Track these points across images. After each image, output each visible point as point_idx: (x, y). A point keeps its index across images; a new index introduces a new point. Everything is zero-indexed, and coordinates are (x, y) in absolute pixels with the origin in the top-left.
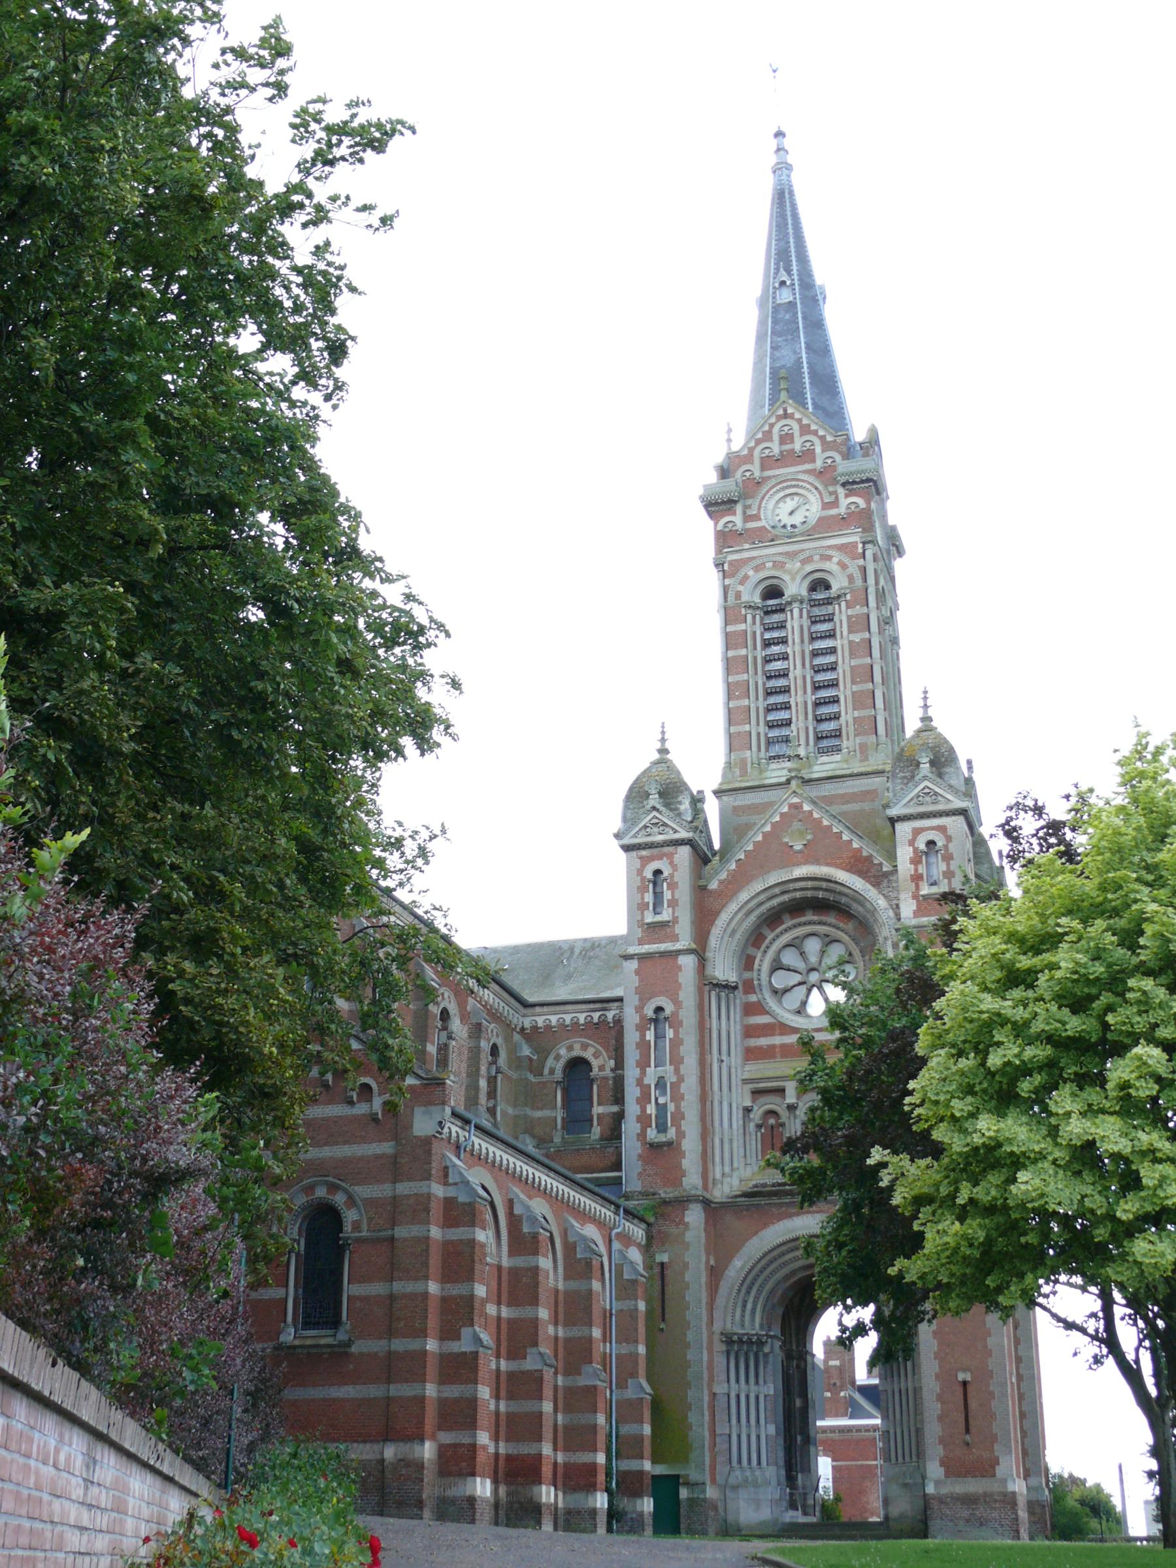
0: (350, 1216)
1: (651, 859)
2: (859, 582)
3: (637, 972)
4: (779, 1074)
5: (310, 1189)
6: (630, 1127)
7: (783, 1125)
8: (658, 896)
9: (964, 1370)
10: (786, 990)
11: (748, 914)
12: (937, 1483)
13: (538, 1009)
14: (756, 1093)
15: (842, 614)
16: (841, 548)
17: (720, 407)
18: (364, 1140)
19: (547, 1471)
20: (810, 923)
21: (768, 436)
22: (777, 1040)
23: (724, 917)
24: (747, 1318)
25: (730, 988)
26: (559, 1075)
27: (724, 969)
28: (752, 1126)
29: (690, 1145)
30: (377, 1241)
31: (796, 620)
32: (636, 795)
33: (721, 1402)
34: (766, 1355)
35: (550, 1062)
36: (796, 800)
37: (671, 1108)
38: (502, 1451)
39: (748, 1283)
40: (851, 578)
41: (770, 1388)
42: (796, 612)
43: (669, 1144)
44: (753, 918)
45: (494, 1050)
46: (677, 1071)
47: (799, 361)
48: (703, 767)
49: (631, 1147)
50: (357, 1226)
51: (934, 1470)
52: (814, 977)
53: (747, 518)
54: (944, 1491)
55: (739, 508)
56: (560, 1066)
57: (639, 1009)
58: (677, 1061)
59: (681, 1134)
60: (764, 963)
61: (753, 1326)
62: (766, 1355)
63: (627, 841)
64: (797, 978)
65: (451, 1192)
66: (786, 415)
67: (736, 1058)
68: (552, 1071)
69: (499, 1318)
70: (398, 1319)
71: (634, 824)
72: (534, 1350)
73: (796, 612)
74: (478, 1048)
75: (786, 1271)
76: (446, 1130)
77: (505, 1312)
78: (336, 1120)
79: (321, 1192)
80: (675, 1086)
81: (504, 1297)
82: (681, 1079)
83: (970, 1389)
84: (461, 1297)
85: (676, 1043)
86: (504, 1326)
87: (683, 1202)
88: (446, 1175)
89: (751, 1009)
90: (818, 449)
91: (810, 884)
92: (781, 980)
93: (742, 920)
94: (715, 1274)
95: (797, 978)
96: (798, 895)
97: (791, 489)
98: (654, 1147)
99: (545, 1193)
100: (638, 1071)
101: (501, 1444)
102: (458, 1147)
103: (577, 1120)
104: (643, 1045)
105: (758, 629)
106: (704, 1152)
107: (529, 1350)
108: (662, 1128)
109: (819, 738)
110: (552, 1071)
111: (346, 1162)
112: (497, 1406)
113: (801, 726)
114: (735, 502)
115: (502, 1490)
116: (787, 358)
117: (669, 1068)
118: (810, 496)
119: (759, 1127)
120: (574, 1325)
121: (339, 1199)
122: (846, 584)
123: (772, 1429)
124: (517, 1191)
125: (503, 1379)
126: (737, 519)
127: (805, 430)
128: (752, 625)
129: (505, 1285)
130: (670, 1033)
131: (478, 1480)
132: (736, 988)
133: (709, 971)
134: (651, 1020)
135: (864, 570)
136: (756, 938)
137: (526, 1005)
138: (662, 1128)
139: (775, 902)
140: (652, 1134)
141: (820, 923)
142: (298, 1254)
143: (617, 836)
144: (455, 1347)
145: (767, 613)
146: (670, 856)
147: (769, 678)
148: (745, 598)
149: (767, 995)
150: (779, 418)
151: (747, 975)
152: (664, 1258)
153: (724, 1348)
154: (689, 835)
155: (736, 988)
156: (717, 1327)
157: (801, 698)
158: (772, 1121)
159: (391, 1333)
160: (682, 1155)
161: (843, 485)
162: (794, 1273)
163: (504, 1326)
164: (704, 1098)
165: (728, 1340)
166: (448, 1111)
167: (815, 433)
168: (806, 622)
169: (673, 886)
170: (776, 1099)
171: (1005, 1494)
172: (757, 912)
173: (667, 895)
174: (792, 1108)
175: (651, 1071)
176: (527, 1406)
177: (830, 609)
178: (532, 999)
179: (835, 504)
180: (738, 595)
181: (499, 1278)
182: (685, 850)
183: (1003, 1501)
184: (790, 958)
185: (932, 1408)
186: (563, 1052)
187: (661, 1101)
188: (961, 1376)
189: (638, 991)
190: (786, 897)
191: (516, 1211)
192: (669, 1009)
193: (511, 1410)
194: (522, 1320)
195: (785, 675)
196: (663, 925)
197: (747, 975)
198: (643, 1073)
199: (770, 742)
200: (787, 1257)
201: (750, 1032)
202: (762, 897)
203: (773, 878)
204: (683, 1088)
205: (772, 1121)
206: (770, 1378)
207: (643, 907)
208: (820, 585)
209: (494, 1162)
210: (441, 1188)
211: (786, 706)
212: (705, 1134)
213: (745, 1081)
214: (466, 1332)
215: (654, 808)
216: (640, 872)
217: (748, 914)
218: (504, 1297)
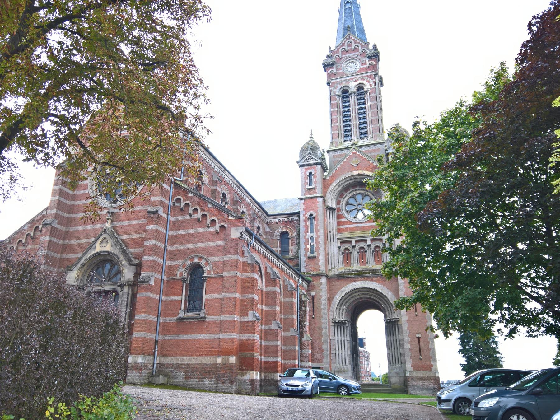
0: (207, 269)
1: (308, 169)
2: (373, 86)
3: (304, 204)
4: (349, 236)
5: (192, 258)
6: (302, 252)
7: (351, 253)
8: (311, 180)
9: (418, 334)
10: (351, 211)
11: (339, 187)
12: (410, 373)
13: (272, 217)
14: (342, 243)
15: (367, 96)
16: (367, 76)
17: (329, 37)
18: (213, 240)
19: (279, 367)
20: (358, 190)
21: (344, 45)
22: (348, 226)
23: (331, 188)
24: (341, 315)
25: (332, 209)
26: (278, 237)
27: (332, 203)
28: (340, 253)
29: (321, 257)
30: (216, 278)
31: (353, 100)
32: (303, 150)
33: (333, 343)
34: (347, 327)
35: (276, 233)
36: (354, 151)
37: (315, 246)
38: (263, 360)
39: (341, 304)
40: (371, 85)
41: (348, 338)
42: (353, 96)
43: (315, 257)
44: (340, 188)
45: (259, 228)
46: (317, 234)
47: (353, 24)
48: (324, 142)
49: (303, 258)
50: (209, 272)
51: (409, 367)
52: (360, 207)
53: (337, 69)
54: (413, 375)
55: (335, 66)
56: (279, 234)
57: (305, 215)
58: (317, 231)
59: (319, 254)
60: (343, 203)
61: (343, 317)
62: (347, 327)
63: (301, 163)
64: (354, 207)
65: (245, 260)
66: (349, 38)
67: (335, 232)
68: (276, 236)
69: (262, 310)
70: (224, 308)
71: (303, 158)
72: (275, 322)
73: (353, 96)
74: (254, 225)
75: (353, 299)
76: (243, 237)
77: (264, 308)
78: (202, 233)
79: (196, 260)
80: (317, 239)
81: (264, 302)
82: (318, 237)
83: (421, 340)
84: (249, 299)
85: (317, 225)
86: (264, 313)
87: (319, 276)
88: (243, 253)
89: (339, 217)
90: (360, 48)
91: (359, 177)
92: (349, 208)
93: (337, 188)
94: (330, 300)
95: (354, 207)
96: (355, 180)
97: (351, 60)
98: (310, 258)
99: (277, 267)
100: (304, 234)
101: (263, 357)
102: (248, 244)
103: (284, 251)
104: (306, 226)
105: (341, 103)
106: (326, 260)
107: (273, 322)
108: (312, 252)
109: (360, 135)
110: (276, 236)
111: (205, 248)
112: (261, 342)
113: (355, 130)
114: (334, 65)
115: (263, 374)
116: (349, 23)
117: (315, 233)
118: (357, 62)
119: (343, 253)
120: (287, 314)
121: (203, 262)
122: (369, 87)
123: (349, 352)
124: (269, 264)
125: (263, 332)
126: (334, 70)
127: (355, 42)
128: (339, 101)
129: (264, 297)
130: (315, 222)
131: (255, 372)
132: (335, 210)
133: (327, 204)
134: (308, 218)
135: (375, 83)
136: (341, 195)
137: (269, 215)
138: (312, 252)
139: (347, 183)
140: (309, 254)
141: (362, 190)
142: (187, 284)
143: (298, 162)
144: (246, 319)
145: (343, 98)
146: (314, 168)
147: (344, 117)
148: (337, 93)
149: (344, 212)
150: (347, 39)
151: (338, 206)
152: (313, 294)
153: (333, 324)
154: (320, 161)
155: (335, 210)
156: (331, 318)
157: (355, 122)
158: (347, 251)
159: (221, 313)
160: (319, 261)
161: (368, 58)
162: (356, 300)
163: (264, 313)
164: (326, 243)
165: (335, 322)
166: (244, 229)
167: (359, 43)
168: (356, 100)
169: (315, 177)
170: (349, 245)
171: (435, 377)
172: (345, 184)
173: (314, 180)
174: (354, 247)
175: (309, 234)
176: (273, 343)
177: (363, 96)
178: (270, 212)
179: (365, 64)
180: (335, 92)
181: (262, 295)
182: (319, 166)
183: (435, 380)
184: (352, 201)
185: (407, 346)
186: (280, 230)
187: (312, 244)
188: (417, 336)
189: (304, 209)
190: (351, 181)
191: (268, 271)
192: (314, 215)
193: (266, 344)
194: (271, 311)
195: (350, 116)
196: (313, 189)
197: (338, 206)
198: (306, 235)
199: (345, 136)
200: (353, 295)
201: (339, 223)
202: (343, 181)
203: (349, 174)
204: (319, 240)
205: (347, 251)
206: (348, 335)
207: (306, 183)
208: (360, 88)
209: (261, 252)
210: (242, 258)
211: (350, 125)
212: (327, 254)
213: (338, 239)
214: (250, 313)
215: (309, 153)
216: (305, 173)
217: (339, 187)
218: (264, 302)
